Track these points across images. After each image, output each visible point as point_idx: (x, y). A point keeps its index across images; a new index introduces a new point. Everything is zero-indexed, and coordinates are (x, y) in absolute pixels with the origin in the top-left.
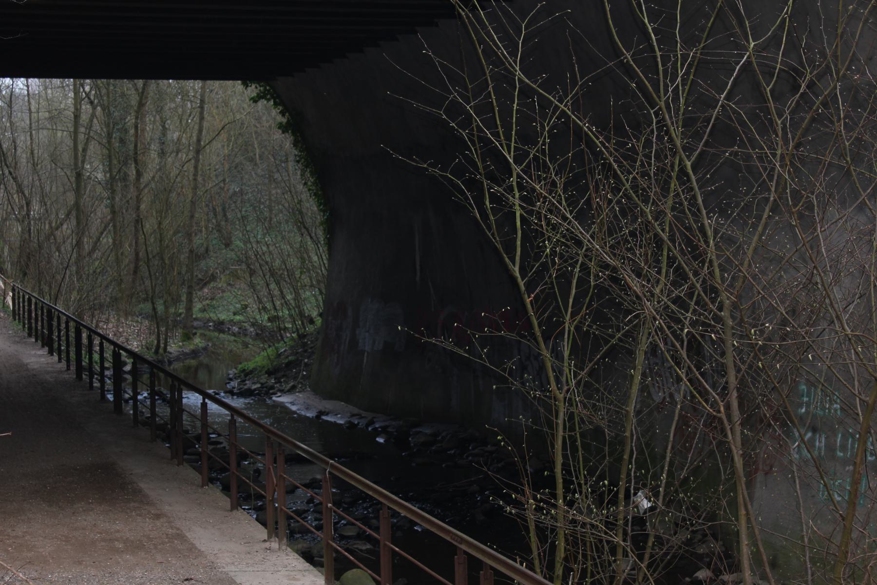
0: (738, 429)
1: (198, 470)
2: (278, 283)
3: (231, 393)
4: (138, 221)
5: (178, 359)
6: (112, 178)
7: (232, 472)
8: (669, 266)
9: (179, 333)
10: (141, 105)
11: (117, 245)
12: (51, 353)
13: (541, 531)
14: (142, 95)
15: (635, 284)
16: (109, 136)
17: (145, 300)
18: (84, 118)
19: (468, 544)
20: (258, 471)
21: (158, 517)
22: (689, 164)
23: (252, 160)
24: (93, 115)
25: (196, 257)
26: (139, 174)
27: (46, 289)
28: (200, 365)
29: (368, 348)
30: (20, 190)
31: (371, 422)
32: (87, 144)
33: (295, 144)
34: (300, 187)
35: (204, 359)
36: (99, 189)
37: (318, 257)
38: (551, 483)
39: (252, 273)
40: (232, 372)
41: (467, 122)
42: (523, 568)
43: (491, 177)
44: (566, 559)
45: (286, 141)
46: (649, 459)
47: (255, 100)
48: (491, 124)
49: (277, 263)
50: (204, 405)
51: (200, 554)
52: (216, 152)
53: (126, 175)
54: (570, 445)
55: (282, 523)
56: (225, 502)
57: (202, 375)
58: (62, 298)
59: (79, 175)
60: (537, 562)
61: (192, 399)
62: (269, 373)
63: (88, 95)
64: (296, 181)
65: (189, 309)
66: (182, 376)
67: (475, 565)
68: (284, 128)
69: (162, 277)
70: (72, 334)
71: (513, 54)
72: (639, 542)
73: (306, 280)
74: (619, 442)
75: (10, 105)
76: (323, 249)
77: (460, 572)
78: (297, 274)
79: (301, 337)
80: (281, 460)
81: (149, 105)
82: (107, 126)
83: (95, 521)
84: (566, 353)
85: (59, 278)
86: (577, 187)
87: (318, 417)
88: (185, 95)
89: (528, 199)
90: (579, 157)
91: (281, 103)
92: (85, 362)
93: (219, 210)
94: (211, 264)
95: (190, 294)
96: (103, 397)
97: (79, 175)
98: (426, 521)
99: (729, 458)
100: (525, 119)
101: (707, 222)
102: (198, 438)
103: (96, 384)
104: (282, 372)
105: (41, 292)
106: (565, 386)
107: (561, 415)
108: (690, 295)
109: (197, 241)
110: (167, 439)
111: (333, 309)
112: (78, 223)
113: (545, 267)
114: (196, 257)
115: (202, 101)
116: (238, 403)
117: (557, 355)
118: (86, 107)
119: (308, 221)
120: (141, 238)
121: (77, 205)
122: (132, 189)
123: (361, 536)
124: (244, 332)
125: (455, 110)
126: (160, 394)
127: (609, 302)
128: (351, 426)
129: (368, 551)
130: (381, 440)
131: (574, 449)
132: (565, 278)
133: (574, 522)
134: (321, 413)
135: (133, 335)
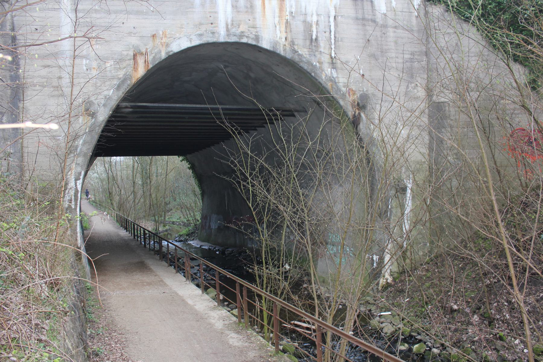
2: (189, 211)
3: (177, 241)
4: (150, 195)
5: (162, 232)
6: (143, 183)
7: (175, 262)
9: (162, 225)
10: (151, 163)
11: (145, 201)
12: (127, 231)
13: (260, 277)
14: (151, 160)
15: (281, 208)
16: (142, 172)
18: (136, 167)
19: (239, 280)
21: (156, 276)
23: (181, 177)
24: (138, 166)
25: (166, 204)
26: (150, 182)
28: (168, 234)
29: (213, 228)
30: (118, 187)
31: (215, 248)
34: (194, 184)
36: (140, 186)
37: (200, 203)
39: (182, 208)
40: (177, 235)
41: (236, 166)
44: (266, 283)
45: (190, 172)
46: (288, 255)
47: (181, 161)
48: (242, 166)
49: (189, 205)
50: (168, 245)
51: (167, 286)
55: (190, 277)
56: (174, 271)
57: (169, 236)
59: (134, 182)
61: (165, 243)
62: (187, 235)
64: (193, 182)
65: (165, 218)
67: (241, 286)
68: (189, 168)
71: (247, 145)
72: (286, 278)
74: (279, 251)
76: (201, 201)
77: (238, 288)
78: (194, 208)
79: (195, 225)
81: (153, 163)
83: (138, 277)
84: (265, 228)
88: (163, 160)
89: (252, 186)
92: (136, 234)
95: (165, 214)
96: (141, 243)
97: (134, 182)
98: (229, 275)
100: (252, 165)
103: (139, 239)
104: (190, 235)
105: (124, 215)
106: (265, 236)
109: (167, 200)
111: (204, 217)
114: (166, 204)
118: (136, 164)
119: (196, 193)
121: (134, 191)
123: (212, 279)
125: (232, 162)
127: (276, 213)
128: (210, 249)
130: (218, 253)
132: (264, 207)
134: (201, 246)
135: (149, 226)
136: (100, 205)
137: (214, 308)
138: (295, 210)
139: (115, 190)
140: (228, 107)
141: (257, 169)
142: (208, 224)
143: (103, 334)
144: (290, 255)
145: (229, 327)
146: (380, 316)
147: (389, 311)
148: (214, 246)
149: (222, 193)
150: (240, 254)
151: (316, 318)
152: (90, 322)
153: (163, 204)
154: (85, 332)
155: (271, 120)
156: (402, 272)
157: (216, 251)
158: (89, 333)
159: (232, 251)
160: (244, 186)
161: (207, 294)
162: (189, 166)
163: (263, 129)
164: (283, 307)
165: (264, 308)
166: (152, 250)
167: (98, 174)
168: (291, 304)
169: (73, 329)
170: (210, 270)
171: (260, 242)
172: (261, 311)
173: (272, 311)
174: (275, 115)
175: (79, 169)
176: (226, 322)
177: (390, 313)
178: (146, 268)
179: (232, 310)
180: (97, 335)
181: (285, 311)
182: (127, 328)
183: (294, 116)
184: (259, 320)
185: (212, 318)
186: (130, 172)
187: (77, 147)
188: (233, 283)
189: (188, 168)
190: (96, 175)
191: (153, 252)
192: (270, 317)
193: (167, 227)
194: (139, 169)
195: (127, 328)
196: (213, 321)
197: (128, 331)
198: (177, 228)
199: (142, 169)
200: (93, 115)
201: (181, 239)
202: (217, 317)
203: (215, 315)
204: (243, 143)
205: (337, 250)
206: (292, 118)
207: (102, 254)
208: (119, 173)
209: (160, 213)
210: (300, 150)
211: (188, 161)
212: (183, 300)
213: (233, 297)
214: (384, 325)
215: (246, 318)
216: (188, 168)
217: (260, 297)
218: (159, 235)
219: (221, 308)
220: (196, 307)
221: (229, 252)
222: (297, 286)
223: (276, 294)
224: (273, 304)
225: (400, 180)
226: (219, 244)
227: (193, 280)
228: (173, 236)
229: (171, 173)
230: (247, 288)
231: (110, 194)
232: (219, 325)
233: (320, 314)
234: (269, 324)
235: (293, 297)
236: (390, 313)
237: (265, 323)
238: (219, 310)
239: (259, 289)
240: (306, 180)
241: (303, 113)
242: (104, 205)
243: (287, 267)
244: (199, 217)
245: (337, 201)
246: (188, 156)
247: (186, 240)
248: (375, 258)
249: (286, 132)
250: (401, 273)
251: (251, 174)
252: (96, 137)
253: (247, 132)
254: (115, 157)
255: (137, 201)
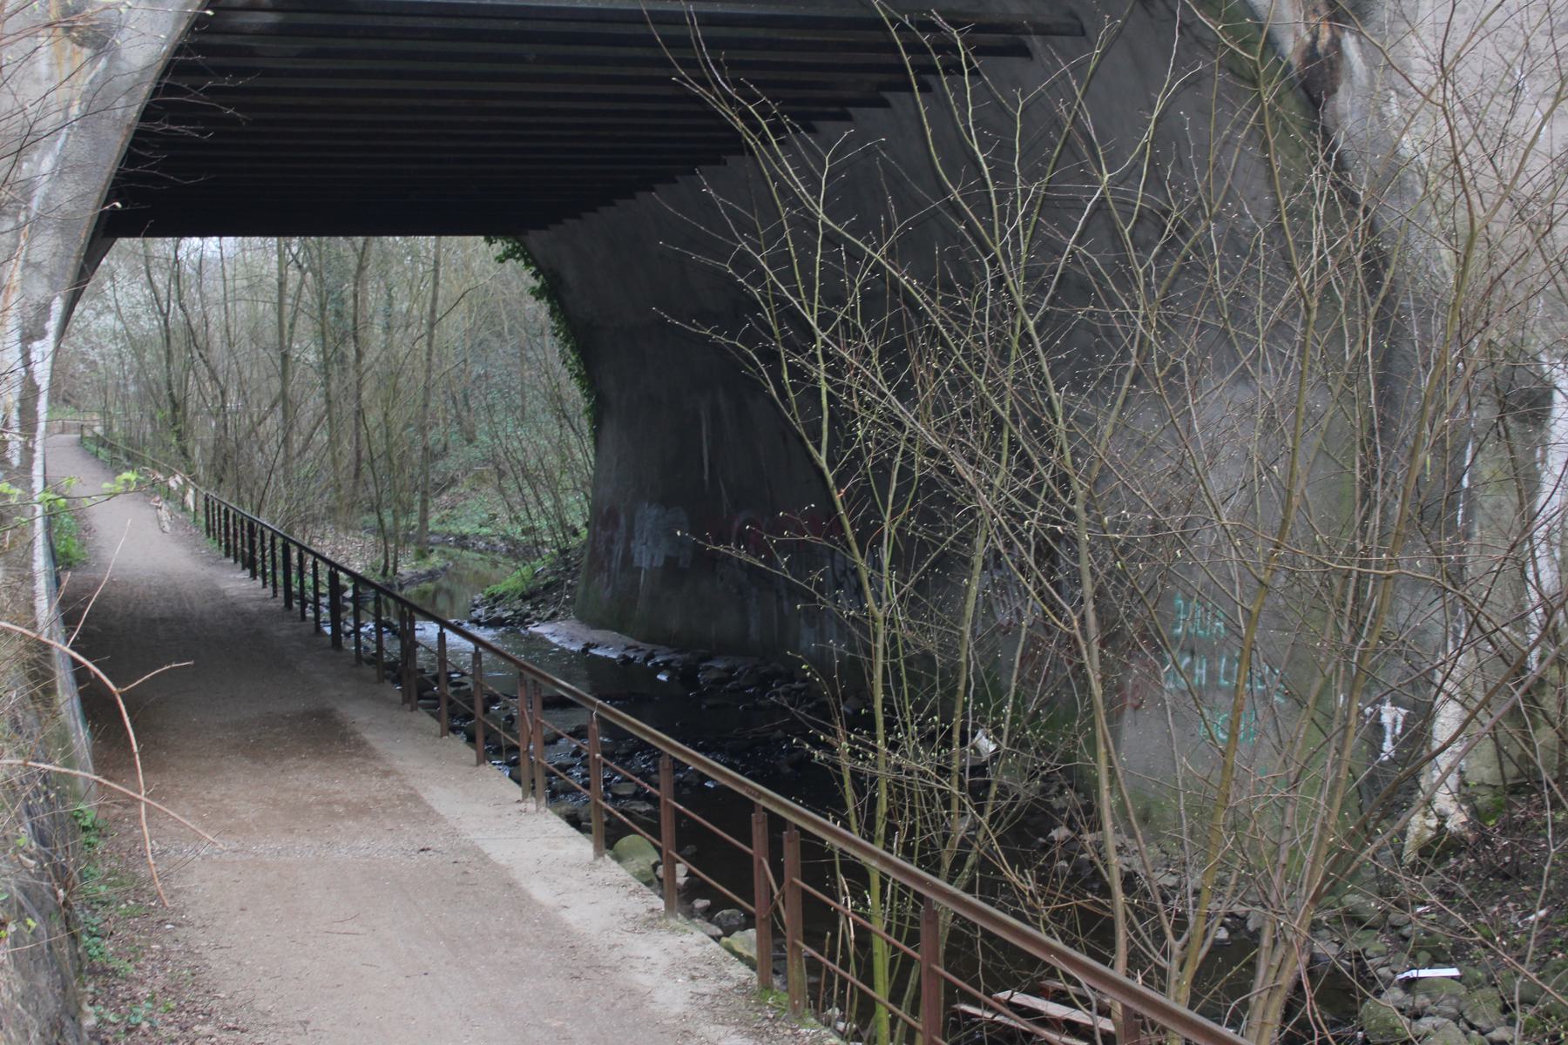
0: (1095, 648)
1: (437, 717)
2: (533, 487)
3: (477, 622)
4: (360, 413)
5: (411, 582)
6: (327, 360)
7: (473, 717)
8: (1012, 452)
9: (412, 549)
10: (361, 268)
11: (334, 442)
12: (253, 576)
13: (859, 789)
14: (362, 255)
16: (322, 307)
17: (370, 510)
18: (291, 286)
19: (768, 799)
20: (511, 718)
21: (386, 774)
22: (1031, 323)
23: (499, 335)
24: (303, 282)
25: (430, 455)
26: (360, 355)
27: (247, 497)
29: (645, 564)
30: (213, 377)
31: (650, 656)
32: (294, 318)
33: (552, 313)
34: (559, 367)
35: (445, 584)
36: (310, 373)
37: (582, 452)
38: (869, 723)
39: (502, 475)
40: (478, 597)
42: (837, 827)
43: (787, 342)
44: (889, 815)
45: (540, 311)
46: (989, 692)
47: (501, 260)
48: (787, 278)
49: (533, 462)
51: (439, 818)
52: (455, 326)
53: (344, 356)
54: (892, 673)
55: (541, 781)
56: (470, 754)
57: (442, 603)
58: (266, 510)
60: (853, 820)
61: (427, 631)
62: (524, 598)
63: (295, 257)
64: (552, 359)
65: (424, 520)
66: (416, 602)
67: (776, 824)
68: (538, 294)
69: (389, 481)
70: (279, 553)
71: (815, 191)
72: (978, 792)
73: (569, 484)
75: (200, 273)
76: (588, 443)
77: (759, 831)
79: (564, 552)
80: (538, 704)
81: (371, 269)
82: (320, 295)
83: (309, 779)
84: (886, 561)
85: (262, 484)
86: (895, 356)
87: (585, 650)
88: (416, 255)
90: (897, 320)
91: (535, 263)
93: (459, 397)
94: (449, 465)
95: (424, 502)
96: (318, 629)
99: (1085, 687)
100: (830, 275)
101: (1054, 395)
102: (436, 679)
103: (310, 614)
104: (538, 596)
105: (240, 501)
106: (884, 602)
107: (881, 638)
108: (1038, 488)
109: (433, 436)
110: (397, 680)
111: (602, 518)
112: (285, 416)
113: (858, 455)
114: (430, 455)
115: (437, 263)
116: (486, 635)
117: (877, 565)
118: (293, 274)
119: (570, 409)
120: (363, 432)
121: (283, 395)
122: (351, 372)
123: (639, 795)
124: (492, 548)
125: (744, 263)
126: (389, 625)
127: (937, 498)
128: (627, 661)
129: (648, 813)
130: (662, 677)
131: (898, 682)
132: (883, 468)
133: (898, 768)
134: (588, 646)
135: (355, 553)
136: (129, 456)
137: (650, 923)
138: (1026, 483)
139: (197, 392)
140: (718, 8)
141: (854, 299)
142: (618, 549)
143: (153, 1028)
144: (999, 692)
145: (715, 1007)
146: (1409, 985)
147: (1449, 964)
148: (648, 648)
149: (684, 397)
150: (764, 683)
151: (1119, 973)
152: (93, 972)
153: (416, 456)
154: (76, 1016)
155: (925, 69)
156: (1522, 785)
157: (658, 669)
158: (90, 1022)
159: (730, 670)
160: (795, 371)
161: (618, 858)
162: (538, 285)
163: (879, 112)
164: (966, 924)
165: (878, 926)
166: (370, 662)
167: (120, 317)
168: (1004, 910)
169: (24, 999)
170: (629, 756)
171: (865, 630)
172: (864, 938)
173: (913, 939)
174: (947, 47)
175: (40, 290)
176: (704, 987)
177: (1454, 972)
178: (344, 739)
179: (728, 933)
180: (128, 1031)
181: (971, 944)
182: (259, 1005)
183: (1024, 52)
184: (851, 977)
185: (640, 964)
186: (265, 308)
187: (28, 187)
188: (734, 810)
189: (533, 291)
190: (109, 320)
191: (371, 671)
192: (902, 968)
193: (435, 560)
194: (307, 296)
195: (259, 1005)
196: (644, 980)
197: (266, 1014)
198: (479, 566)
199: (325, 295)
200: (98, 40)
201: (499, 612)
202: (665, 961)
203: (654, 953)
204: (797, 174)
205: (1213, 675)
206: (1016, 63)
207: (147, 677)
208: (215, 315)
209: (405, 496)
210: (1054, 208)
211: (530, 259)
212: (510, 885)
213: (739, 874)
214: (1426, 1023)
215: (797, 974)
216: (533, 291)
217: (858, 875)
218: (398, 593)
219: (678, 921)
220: (570, 917)
221: (714, 676)
222: (1026, 831)
223: (933, 866)
224: (916, 909)
225: (1519, 354)
226: (668, 641)
227: (553, 796)
228: (462, 602)
229: (455, 317)
230: (804, 833)
231: (175, 406)
232: (672, 997)
233: (1136, 961)
234: (896, 997)
235: (1012, 876)
236: (1454, 972)
237: (881, 992)
238: (673, 930)
239: (856, 837)
240: (1084, 350)
241: (1067, 41)
242: (148, 456)
243: (987, 745)
244: (577, 513)
245: (1217, 452)
246: (534, 238)
247: (522, 619)
248: (1391, 715)
249: (994, 123)
250: (1515, 790)
251: (824, 321)
252: (115, 143)
253: (810, 130)
254: (196, 241)
255: (297, 442)
